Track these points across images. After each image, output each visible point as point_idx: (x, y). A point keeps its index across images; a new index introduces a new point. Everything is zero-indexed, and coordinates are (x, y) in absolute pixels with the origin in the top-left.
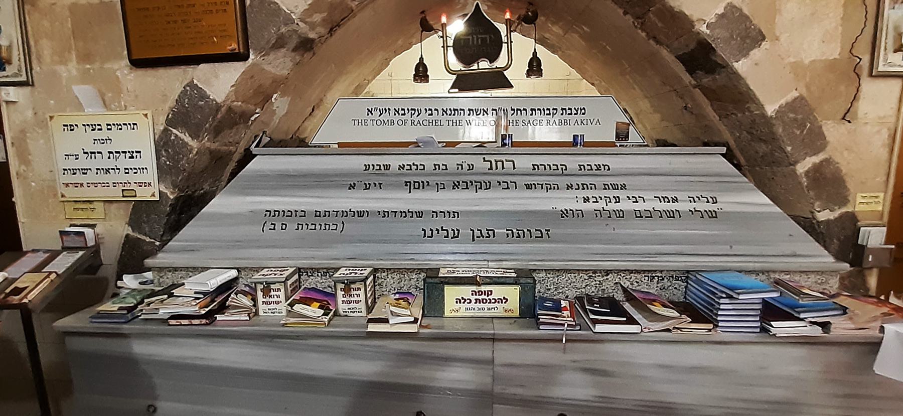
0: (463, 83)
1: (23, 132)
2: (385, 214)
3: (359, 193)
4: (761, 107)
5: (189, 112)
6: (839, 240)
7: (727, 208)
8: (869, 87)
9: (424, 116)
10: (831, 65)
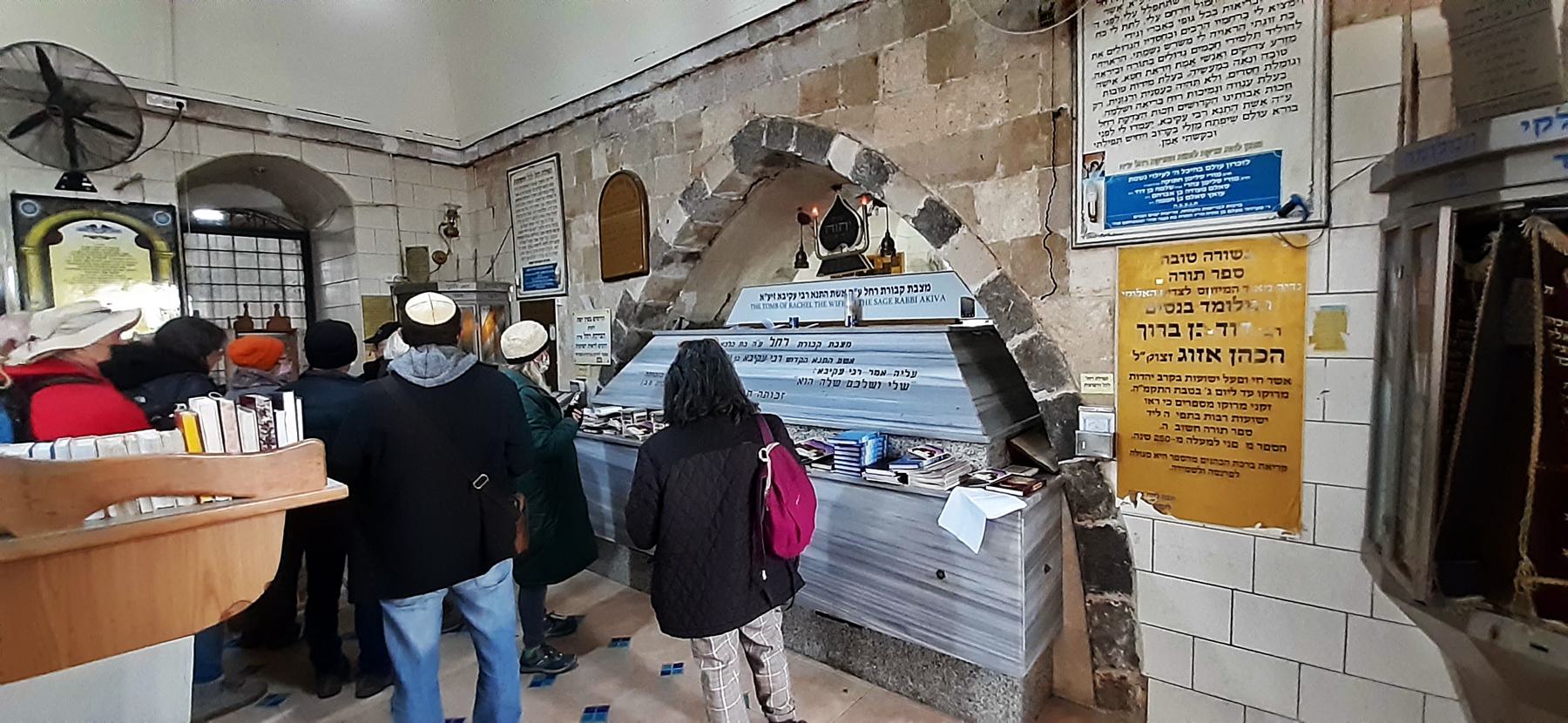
0: (828, 268)
5: (625, 311)
6: (1061, 423)
8: (1075, 260)
10: (1033, 241)
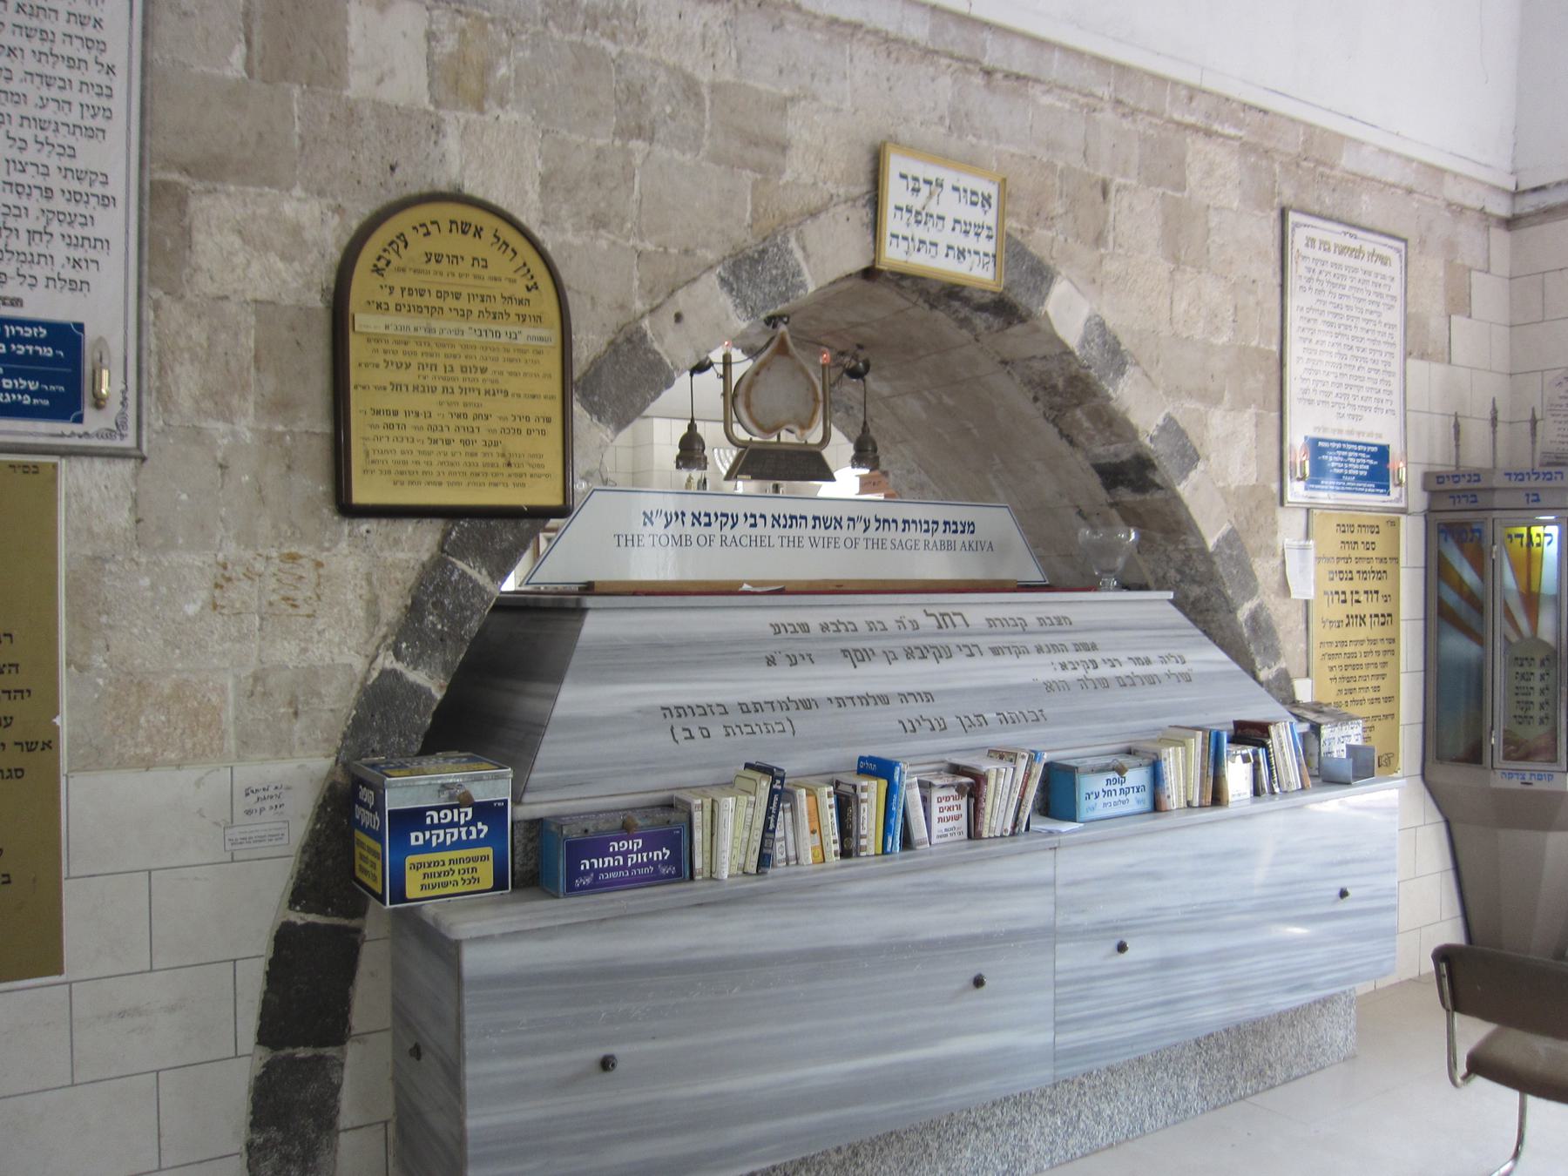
1: (98, 560)
2: (841, 701)
3: (783, 670)
4: (1201, 540)
7: (1197, 668)
9: (743, 528)
